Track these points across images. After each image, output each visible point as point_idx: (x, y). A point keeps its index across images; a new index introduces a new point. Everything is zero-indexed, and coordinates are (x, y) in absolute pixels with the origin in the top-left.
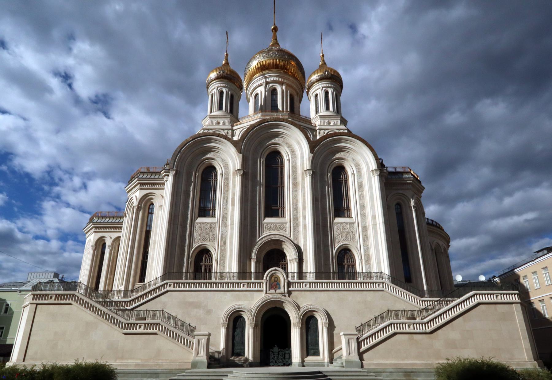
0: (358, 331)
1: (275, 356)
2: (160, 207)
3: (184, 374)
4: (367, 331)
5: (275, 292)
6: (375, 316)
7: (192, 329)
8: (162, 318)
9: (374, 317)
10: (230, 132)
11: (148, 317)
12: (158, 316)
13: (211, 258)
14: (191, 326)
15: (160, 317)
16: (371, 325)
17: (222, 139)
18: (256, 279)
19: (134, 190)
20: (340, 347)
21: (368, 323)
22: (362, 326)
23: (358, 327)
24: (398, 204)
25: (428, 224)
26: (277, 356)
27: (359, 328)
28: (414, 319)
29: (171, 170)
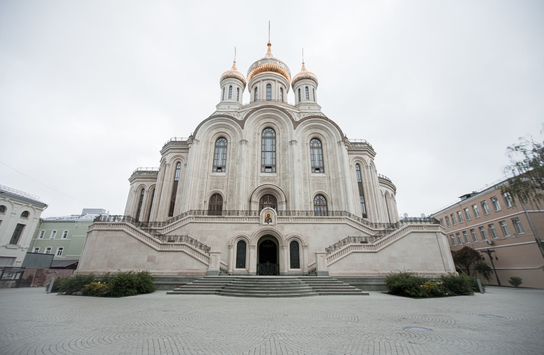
9: (339, 241)
11: (177, 240)
18: (287, 215)
19: (167, 153)
24: (357, 164)
25: (379, 178)
26: (269, 269)
28: (367, 242)
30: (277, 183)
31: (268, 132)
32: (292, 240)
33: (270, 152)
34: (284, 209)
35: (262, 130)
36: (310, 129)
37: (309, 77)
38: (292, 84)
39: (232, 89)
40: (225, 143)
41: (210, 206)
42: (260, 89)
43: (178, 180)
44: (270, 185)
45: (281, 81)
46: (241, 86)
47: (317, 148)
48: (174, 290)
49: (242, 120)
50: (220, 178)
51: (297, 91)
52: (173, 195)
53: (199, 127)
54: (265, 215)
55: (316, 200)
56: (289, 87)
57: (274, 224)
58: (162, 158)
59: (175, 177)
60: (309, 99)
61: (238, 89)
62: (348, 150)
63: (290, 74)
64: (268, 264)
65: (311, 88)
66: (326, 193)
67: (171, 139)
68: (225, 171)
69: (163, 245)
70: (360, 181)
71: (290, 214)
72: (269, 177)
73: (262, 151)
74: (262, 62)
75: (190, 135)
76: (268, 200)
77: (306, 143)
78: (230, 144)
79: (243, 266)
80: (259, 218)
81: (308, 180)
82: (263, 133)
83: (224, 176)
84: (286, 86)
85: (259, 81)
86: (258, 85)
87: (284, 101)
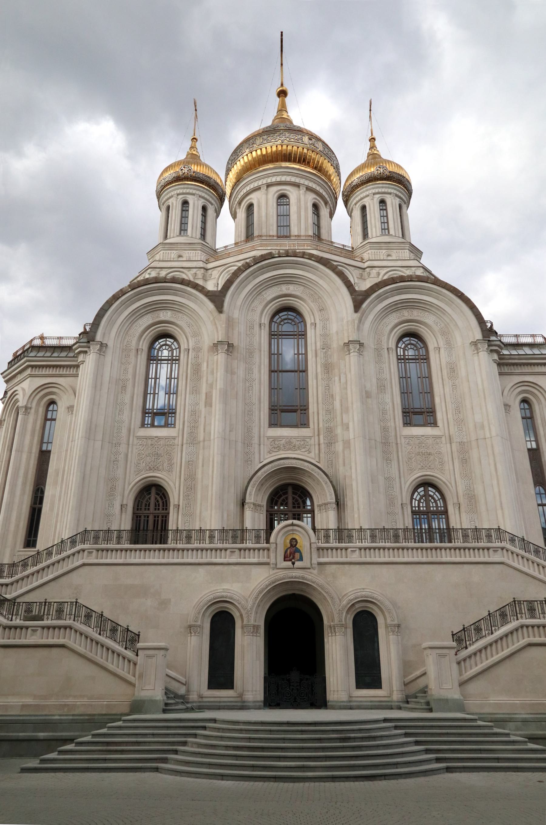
0: (456, 640)
1: (293, 689)
2: (68, 408)
3: (120, 723)
4: (474, 640)
5: (292, 567)
6: (489, 611)
7: (133, 637)
8: (75, 617)
9: (487, 613)
10: (200, 273)
11: (48, 614)
12: (68, 613)
13: (166, 501)
14: (131, 631)
15: (70, 614)
16: (481, 630)
17: (189, 289)
19: (20, 377)
20: (423, 669)
21: (477, 624)
22: (465, 631)
23: (457, 633)
24: (525, 401)
26: (297, 689)
27: (459, 635)
29: (91, 343)
30: (312, 455)
31: (286, 321)
32: (359, 607)
33: (284, 369)
34: (332, 524)
35: (272, 314)
36: (397, 310)
37: (388, 174)
38: (343, 195)
39: (188, 211)
40: (175, 351)
41: (136, 518)
42: (259, 206)
43: (49, 449)
44: (295, 458)
45: (314, 186)
46: (213, 201)
47: (408, 359)
48: (43, 761)
49: (215, 289)
50: (162, 442)
51: (357, 213)
52: (38, 490)
53: (106, 311)
54: (285, 541)
55: (418, 499)
56: (336, 203)
57: (309, 565)
58: (6, 393)
59: (42, 442)
60: (389, 232)
61: (204, 209)
62: (499, 365)
63: (337, 168)
64: (295, 676)
65: (392, 203)
66: (444, 480)
67: (32, 340)
68: (175, 424)
69: (10, 628)
70: (534, 446)
71: (350, 537)
72: (291, 437)
73: (273, 371)
74: (265, 137)
75: (82, 330)
76: (290, 501)
77: (386, 348)
78: (186, 353)
79: (228, 684)
80: (268, 549)
81: (394, 445)
82: (273, 323)
83: (174, 438)
84: (328, 199)
85: (258, 189)
86: (254, 198)
87: (324, 236)
